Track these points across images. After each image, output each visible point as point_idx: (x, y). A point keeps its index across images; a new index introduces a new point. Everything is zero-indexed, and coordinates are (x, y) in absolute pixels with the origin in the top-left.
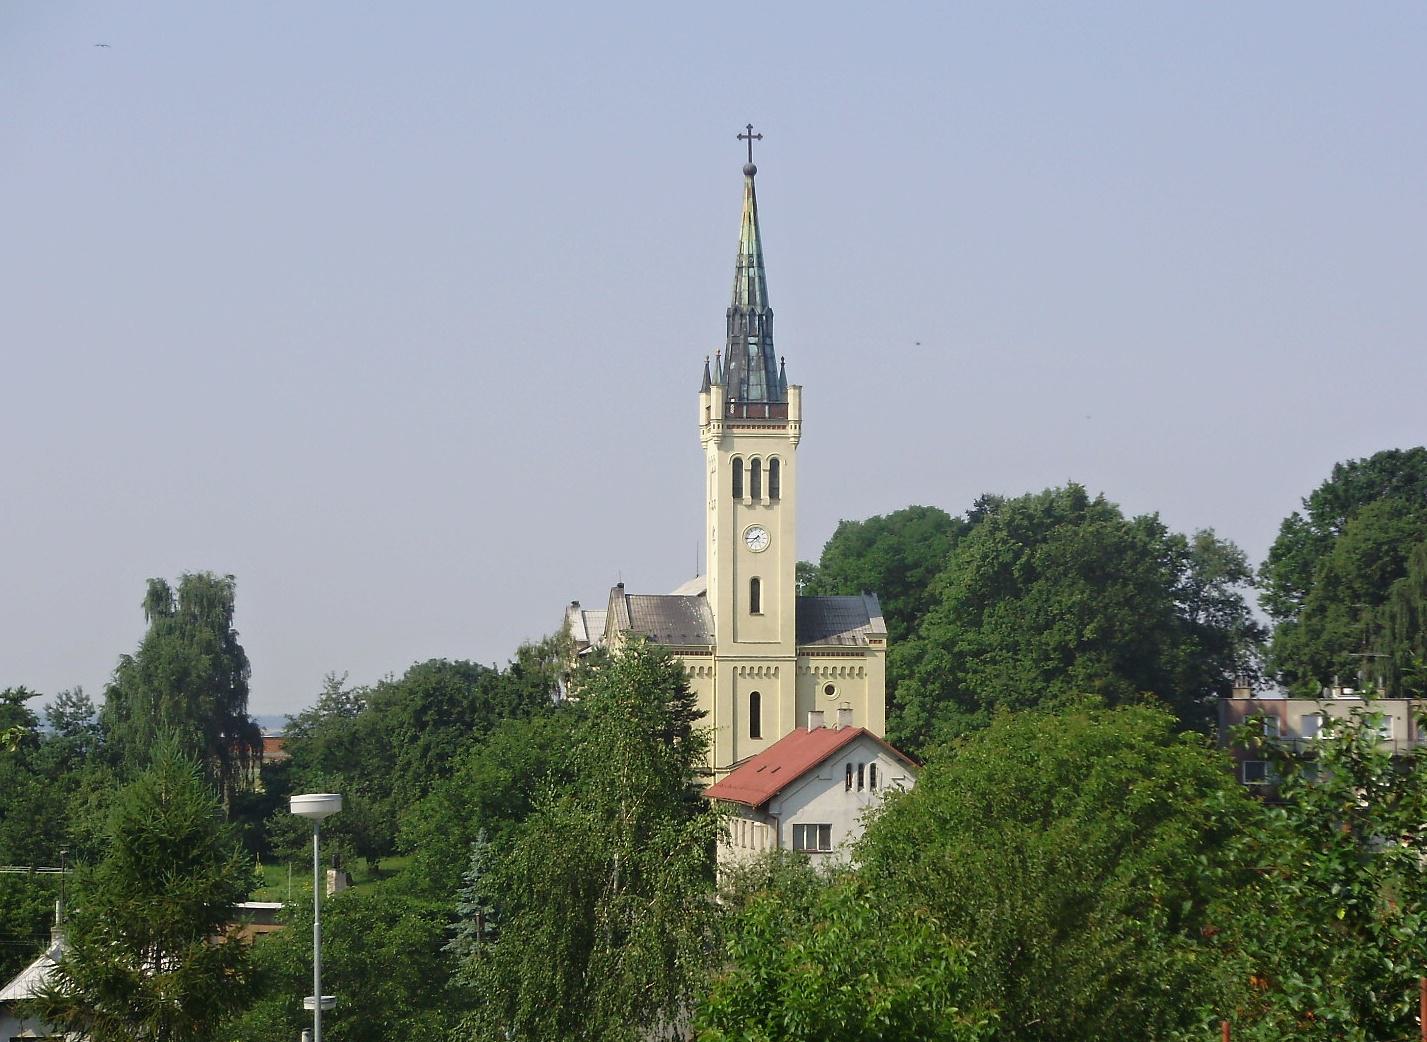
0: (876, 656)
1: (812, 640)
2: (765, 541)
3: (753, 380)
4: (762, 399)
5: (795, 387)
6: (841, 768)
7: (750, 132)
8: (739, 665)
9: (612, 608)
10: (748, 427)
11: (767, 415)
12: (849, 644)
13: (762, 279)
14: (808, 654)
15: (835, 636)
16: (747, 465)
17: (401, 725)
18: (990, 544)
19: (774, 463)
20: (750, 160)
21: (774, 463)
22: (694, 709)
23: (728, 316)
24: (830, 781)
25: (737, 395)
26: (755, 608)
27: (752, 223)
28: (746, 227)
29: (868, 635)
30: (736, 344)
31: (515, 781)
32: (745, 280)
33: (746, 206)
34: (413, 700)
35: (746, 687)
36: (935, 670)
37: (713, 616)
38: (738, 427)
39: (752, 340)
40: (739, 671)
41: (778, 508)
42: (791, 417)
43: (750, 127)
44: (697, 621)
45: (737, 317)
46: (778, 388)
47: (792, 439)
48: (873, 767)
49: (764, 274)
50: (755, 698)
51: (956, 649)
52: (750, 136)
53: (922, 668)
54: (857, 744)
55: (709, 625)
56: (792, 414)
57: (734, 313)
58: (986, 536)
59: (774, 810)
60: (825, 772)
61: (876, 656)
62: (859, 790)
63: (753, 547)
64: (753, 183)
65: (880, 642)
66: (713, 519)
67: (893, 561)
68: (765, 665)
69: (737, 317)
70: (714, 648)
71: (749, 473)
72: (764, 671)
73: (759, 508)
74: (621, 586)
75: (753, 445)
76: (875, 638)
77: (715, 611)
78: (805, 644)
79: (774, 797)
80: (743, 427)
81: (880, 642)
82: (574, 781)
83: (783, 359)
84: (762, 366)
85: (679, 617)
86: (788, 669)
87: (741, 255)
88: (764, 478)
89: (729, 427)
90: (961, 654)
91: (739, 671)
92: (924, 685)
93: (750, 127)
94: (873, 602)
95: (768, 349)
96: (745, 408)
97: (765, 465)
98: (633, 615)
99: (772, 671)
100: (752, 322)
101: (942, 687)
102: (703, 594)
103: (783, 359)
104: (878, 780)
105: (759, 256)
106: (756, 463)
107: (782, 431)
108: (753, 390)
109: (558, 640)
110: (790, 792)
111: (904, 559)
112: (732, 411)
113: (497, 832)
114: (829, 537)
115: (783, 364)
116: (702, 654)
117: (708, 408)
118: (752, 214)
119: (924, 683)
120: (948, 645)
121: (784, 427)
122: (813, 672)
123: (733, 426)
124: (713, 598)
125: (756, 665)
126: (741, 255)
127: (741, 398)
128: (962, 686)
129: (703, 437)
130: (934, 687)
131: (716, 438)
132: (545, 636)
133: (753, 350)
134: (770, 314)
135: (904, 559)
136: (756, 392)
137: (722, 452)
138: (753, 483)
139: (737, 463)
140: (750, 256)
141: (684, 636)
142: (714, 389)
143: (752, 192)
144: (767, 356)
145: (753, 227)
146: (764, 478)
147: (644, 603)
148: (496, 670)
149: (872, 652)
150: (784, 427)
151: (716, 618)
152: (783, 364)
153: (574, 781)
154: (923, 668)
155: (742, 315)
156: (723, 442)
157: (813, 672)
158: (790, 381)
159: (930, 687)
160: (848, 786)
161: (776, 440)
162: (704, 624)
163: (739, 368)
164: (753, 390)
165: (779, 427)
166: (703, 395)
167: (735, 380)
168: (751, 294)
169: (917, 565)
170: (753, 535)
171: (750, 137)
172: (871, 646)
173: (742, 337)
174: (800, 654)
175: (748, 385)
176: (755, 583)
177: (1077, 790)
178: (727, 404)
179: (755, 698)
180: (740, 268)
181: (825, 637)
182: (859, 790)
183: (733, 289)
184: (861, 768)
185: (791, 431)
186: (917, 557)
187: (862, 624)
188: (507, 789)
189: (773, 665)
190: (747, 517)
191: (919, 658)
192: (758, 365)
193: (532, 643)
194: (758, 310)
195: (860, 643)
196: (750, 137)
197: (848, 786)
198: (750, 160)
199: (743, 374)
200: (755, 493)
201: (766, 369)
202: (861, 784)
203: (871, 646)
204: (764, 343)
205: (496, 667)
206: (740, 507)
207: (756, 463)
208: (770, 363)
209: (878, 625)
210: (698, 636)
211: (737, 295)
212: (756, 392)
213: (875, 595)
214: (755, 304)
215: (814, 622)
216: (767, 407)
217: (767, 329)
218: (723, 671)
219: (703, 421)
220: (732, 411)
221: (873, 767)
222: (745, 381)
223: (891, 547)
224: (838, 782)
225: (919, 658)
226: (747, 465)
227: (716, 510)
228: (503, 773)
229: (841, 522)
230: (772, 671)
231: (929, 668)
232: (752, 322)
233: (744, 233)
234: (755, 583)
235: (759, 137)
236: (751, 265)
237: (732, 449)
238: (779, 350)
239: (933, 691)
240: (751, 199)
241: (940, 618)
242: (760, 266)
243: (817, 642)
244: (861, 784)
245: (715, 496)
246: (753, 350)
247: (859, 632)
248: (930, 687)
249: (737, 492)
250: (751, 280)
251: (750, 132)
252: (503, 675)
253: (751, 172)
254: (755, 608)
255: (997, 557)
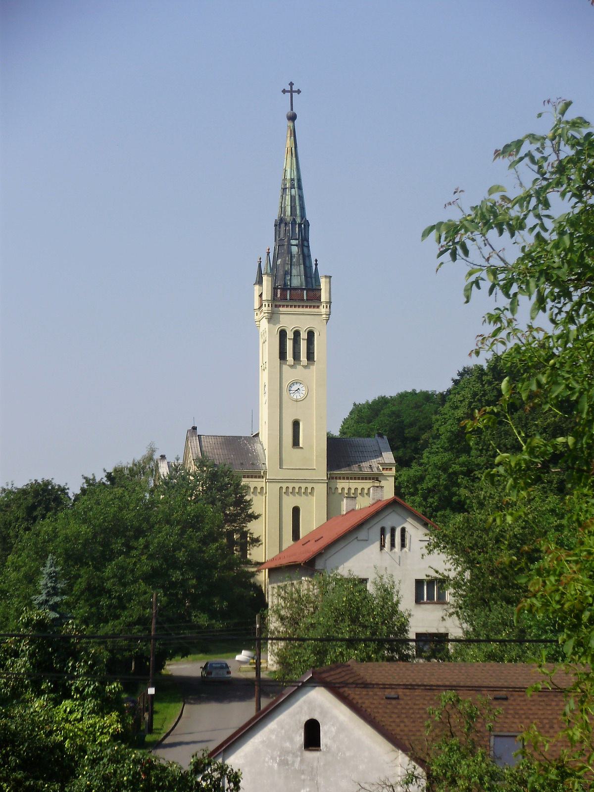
0: (388, 480)
1: (339, 467)
2: (302, 395)
3: (294, 272)
4: (301, 285)
5: (326, 277)
6: (376, 530)
7: (291, 88)
8: (284, 486)
9: (188, 445)
10: (291, 306)
11: (305, 298)
12: (367, 471)
13: (301, 198)
14: (336, 478)
15: (357, 465)
16: (290, 335)
17: (17, 519)
18: (479, 385)
19: (311, 334)
20: (292, 109)
21: (311, 334)
22: (250, 511)
23: (276, 225)
24: (367, 541)
25: (282, 283)
26: (296, 443)
27: (294, 155)
28: (289, 159)
29: (382, 464)
30: (282, 245)
31: (95, 535)
32: (288, 198)
33: (289, 143)
34: (25, 499)
35: (290, 502)
36: (434, 486)
37: (264, 450)
38: (283, 306)
39: (294, 242)
40: (284, 490)
41: (314, 368)
42: (323, 299)
43: (291, 84)
44: (252, 453)
45: (283, 225)
46: (313, 280)
47: (324, 316)
48: (403, 530)
49: (302, 193)
50: (296, 511)
51: (451, 470)
52: (291, 91)
53: (424, 486)
54: (390, 510)
55: (261, 456)
56: (324, 297)
57: (280, 223)
58: (475, 381)
59: (319, 565)
60: (362, 534)
61: (388, 480)
62: (391, 550)
63: (295, 397)
64: (294, 126)
65: (391, 469)
66: (264, 377)
67: (395, 423)
68: (303, 486)
69: (283, 225)
70: (265, 473)
71: (292, 342)
72: (303, 490)
73: (299, 368)
74: (194, 428)
75: (295, 319)
76: (387, 467)
77: (266, 446)
78: (334, 471)
79: (319, 554)
80: (287, 306)
81: (391, 469)
82: (146, 536)
83: (316, 261)
84: (301, 261)
85: (240, 447)
86: (321, 490)
87: (285, 179)
88: (303, 345)
89: (276, 306)
90: (455, 473)
91: (284, 490)
92: (425, 499)
93: (291, 84)
94: (384, 442)
95: (305, 249)
96: (288, 292)
97: (304, 335)
98: (204, 449)
99: (309, 491)
100: (293, 230)
101: (440, 499)
102: (257, 435)
103: (316, 261)
104: (407, 541)
105: (299, 180)
106: (297, 334)
107: (316, 310)
108: (295, 281)
109: (144, 462)
110: (333, 550)
111: (403, 422)
112: (279, 295)
113: (77, 579)
114: (346, 415)
115: (316, 265)
116: (256, 477)
117: (261, 296)
118: (293, 149)
119: (425, 498)
120: (444, 468)
121: (318, 307)
122: (340, 491)
123: (280, 306)
124: (264, 438)
125: (297, 486)
126: (285, 179)
127: (285, 284)
128: (455, 499)
129: (256, 318)
130: (433, 500)
131: (266, 314)
132: (134, 460)
133: (295, 250)
134: (307, 224)
135: (403, 422)
136: (297, 281)
137: (272, 325)
138: (294, 348)
139: (283, 334)
140: (292, 180)
141: (242, 464)
142: (265, 278)
143: (294, 133)
144: (305, 256)
145: (294, 159)
146: (303, 345)
147: (212, 441)
148: (94, 479)
149: (385, 477)
150: (318, 307)
151: (266, 452)
152: (316, 265)
153: (146, 536)
154: (427, 484)
155: (286, 224)
156: (272, 318)
157: (340, 491)
158: (321, 273)
159: (430, 500)
160: (382, 546)
161: (313, 317)
162: (257, 456)
163: (284, 263)
164: (295, 281)
165: (314, 307)
166: (257, 287)
167: (281, 273)
168: (293, 208)
169: (411, 425)
170: (295, 388)
171: (291, 92)
172: (384, 472)
173: (286, 240)
174: (330, 478)
175: (291, 276)
176: (296, 424)
177: (513, 631)
178: (275, 289)
179: (296, 511)
180: (284, 189)
181: (349, 465)
182: (391, 550)
183: (280, 205)
184: (393, 530)
185: (323, 310)
186: (412, 419)
187: (376, 457)
188: (86, 544)
189: (310, 486)
190: (290, 374)
191: (421, 479)
192: (298, 260)
193: (124, 464)
194: (298, 220)
195: (375, 471)
196: (291, 92)
197: (382, 546)
198: (292, 109)
199: (287, 267)
200: (296, 356)
201: (304, 264)
202: (393, 545)
203: (384, 472)
204: (303, 245)
205: (94, 477)
206: (285, 367)
207: (297, 334)
208: (307, 259)
209: (388, 457)
210: (253, 464)
211: (282, 209)
212: (297, 281)
213: (385, 437)
214: (296, 215)
215: (341, 454)
216: (305, 292)
217: (305, 234)
218: (272, 490)
219: (257, 306)
220: (279, 295)
221: (403, 530)
222: (288, 273)
223: (393, 413)
224: (373, 543)
225: (421, 479)
226: (290, 335)
227: (267, 371)
228: (84, 528)
229: (355, 404)
230: (309, 491)
231: (430, 485)
232: (293, 230)
233: (287, 163)
234: (296, 424)
235: (299, 92)
236: (292, 187)
237: (279, 322)
238: (315, 251)
239: (433, 503)
240: (292, 138)
241: (437, 448)
242: (300, 188)
243: (343, 469)
244: (393, 545)
245: (266, 359)
246: (295, 250)
247: (374, 462)
248: (430, 500)
249: (283, 355)
250: (293, 198)
251: (291, 88)
252: (99, 482)
253: (292, 118)
254: (296, 443)
255: (484, 395)
